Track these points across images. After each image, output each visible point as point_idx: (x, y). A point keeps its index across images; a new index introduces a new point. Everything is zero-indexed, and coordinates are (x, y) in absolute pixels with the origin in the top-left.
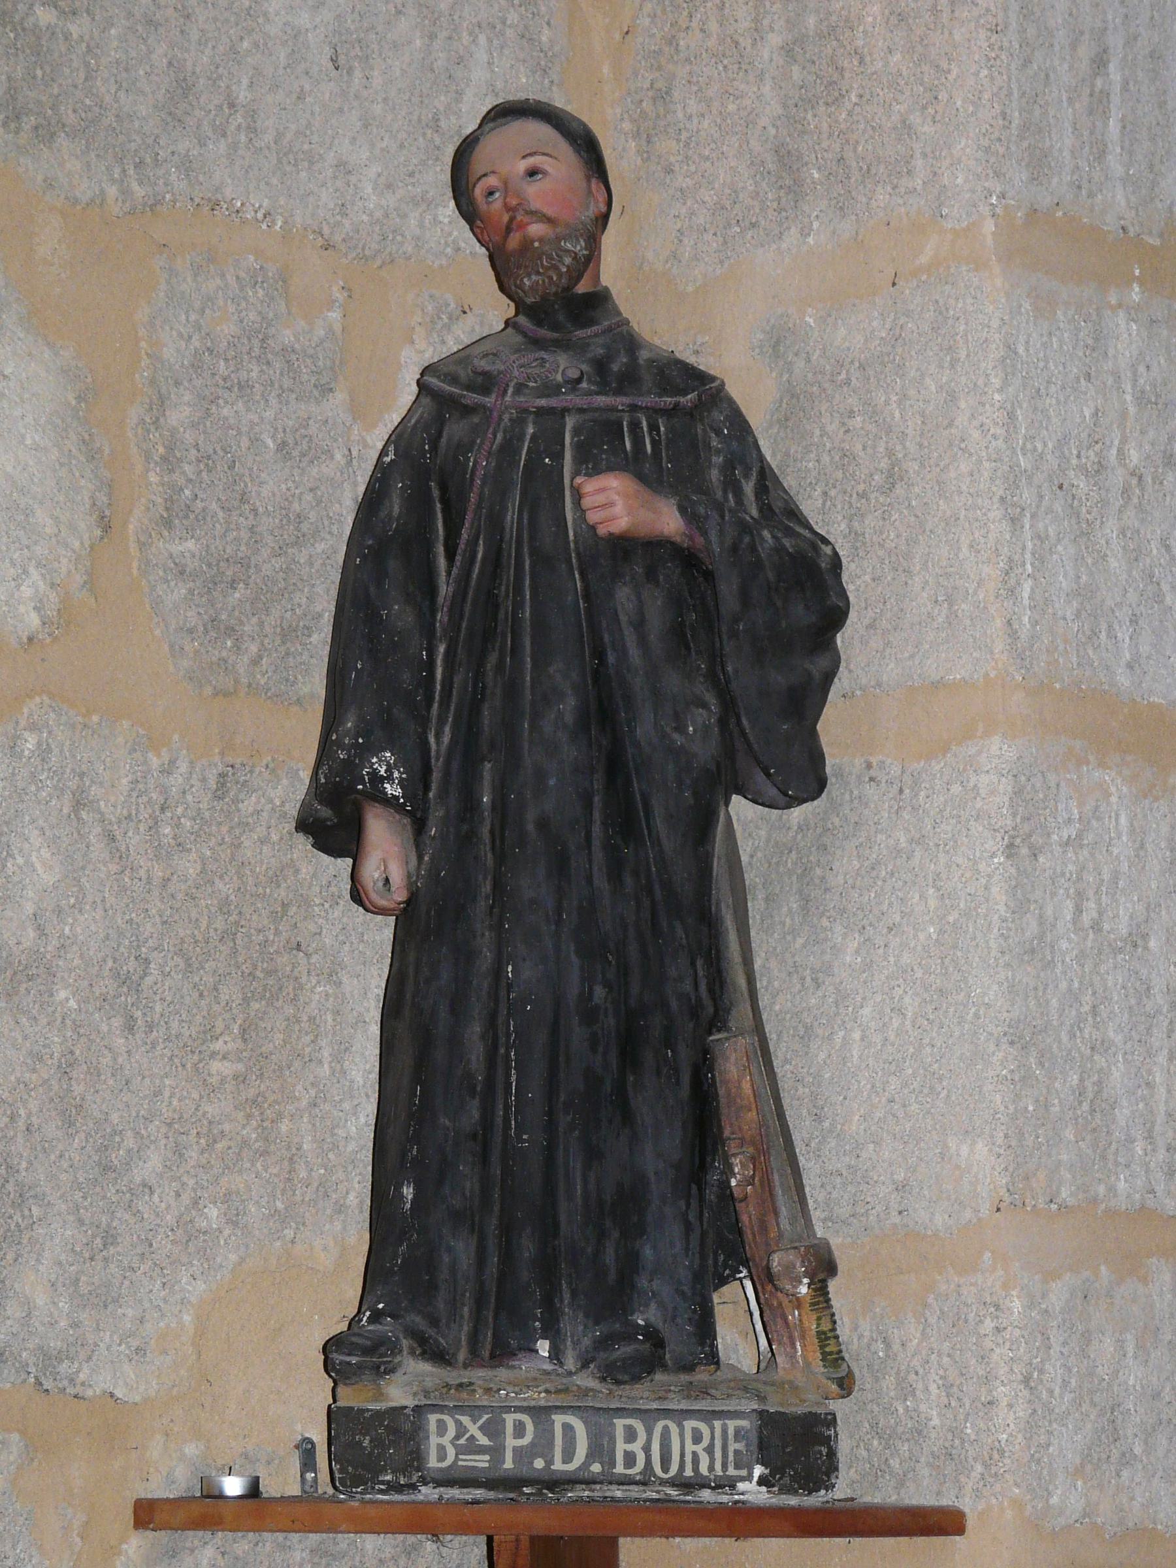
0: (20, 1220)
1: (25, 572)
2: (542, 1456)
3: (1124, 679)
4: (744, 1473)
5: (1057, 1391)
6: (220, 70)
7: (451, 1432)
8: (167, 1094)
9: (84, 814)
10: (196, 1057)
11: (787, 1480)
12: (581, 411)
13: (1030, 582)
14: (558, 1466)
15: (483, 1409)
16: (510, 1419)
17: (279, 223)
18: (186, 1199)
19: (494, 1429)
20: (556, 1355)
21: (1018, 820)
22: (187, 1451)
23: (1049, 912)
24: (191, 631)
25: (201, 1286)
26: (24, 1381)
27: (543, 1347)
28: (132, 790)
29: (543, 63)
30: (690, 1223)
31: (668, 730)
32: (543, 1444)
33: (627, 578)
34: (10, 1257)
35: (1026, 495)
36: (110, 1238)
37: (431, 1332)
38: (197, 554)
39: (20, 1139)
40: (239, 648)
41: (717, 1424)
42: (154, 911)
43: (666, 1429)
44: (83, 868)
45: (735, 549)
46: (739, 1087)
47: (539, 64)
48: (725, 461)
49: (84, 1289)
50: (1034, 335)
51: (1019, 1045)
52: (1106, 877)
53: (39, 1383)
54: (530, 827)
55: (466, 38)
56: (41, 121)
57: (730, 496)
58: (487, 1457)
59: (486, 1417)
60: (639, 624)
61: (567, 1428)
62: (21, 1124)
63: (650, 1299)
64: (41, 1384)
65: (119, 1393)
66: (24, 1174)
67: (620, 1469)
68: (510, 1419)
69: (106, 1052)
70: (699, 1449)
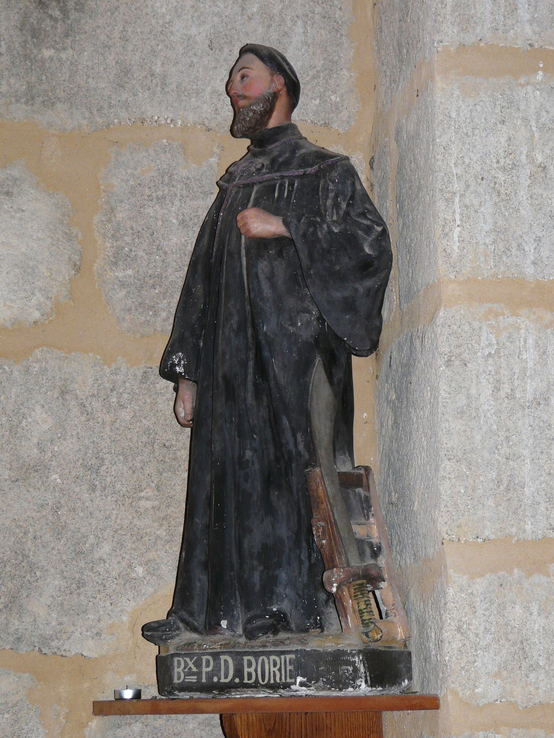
0: (29, 578)
1: (33, 294)
2: (217, 676)
3: (530, 270)
4: (293, 681)
5: (481, 635)
6: (146, 61)
7: (182, 666)
8: (113, 517)
9: (67, 397)
10: (130, 500)
11: (321, 684)
12: (260, 183)
13: (459, 229)
14: (223, 680)
15: (194, 654)
16: (204, 658)
17: (180, 123)
18: (124, 564)
19: (198, 664)
20: (231, 627)
21: (452, 348)
22: (126, 679)
23: (473, 391)
24: (130, 310)
25: (133, 603)
26: (33, 650)
27: (224, 624)
28: (94, 383)
29: (336, 27)
30: (302, 560)
31: (286, 326)
32: (216, 671)
33: (266, 257)
34: (25, 595)
35: (456, 186)
36: (81, 584)
37: (191, 619)
38: (133, 275)
39: (29, 542)
40: (156, 315)
41: (283, 657)
42: (106, 436)
43: (263, 660)
44: (66, 420)
45: (304, 235)
46: (317, 493)
47: (334, 28)
48: (335, 195)
49: (66, 607)
50: (463, 107)
51: (454, 460)
52: (517, 371)
53: (40, 650)
54: (220, 379)
55: (289, 23)
56: (46, 98)
57: (335, 211)
58: (196, 677)
59: (195, 658)
60: (271, 278)
61: (226, 661)
62: (30, 536)
63: (284, 598)
64: (41, 651)
65: (85, 654)
66: (32, 557)
67: (246, 681)
68: (204, 658)
69: (78, 501)
70: (276, 669)
